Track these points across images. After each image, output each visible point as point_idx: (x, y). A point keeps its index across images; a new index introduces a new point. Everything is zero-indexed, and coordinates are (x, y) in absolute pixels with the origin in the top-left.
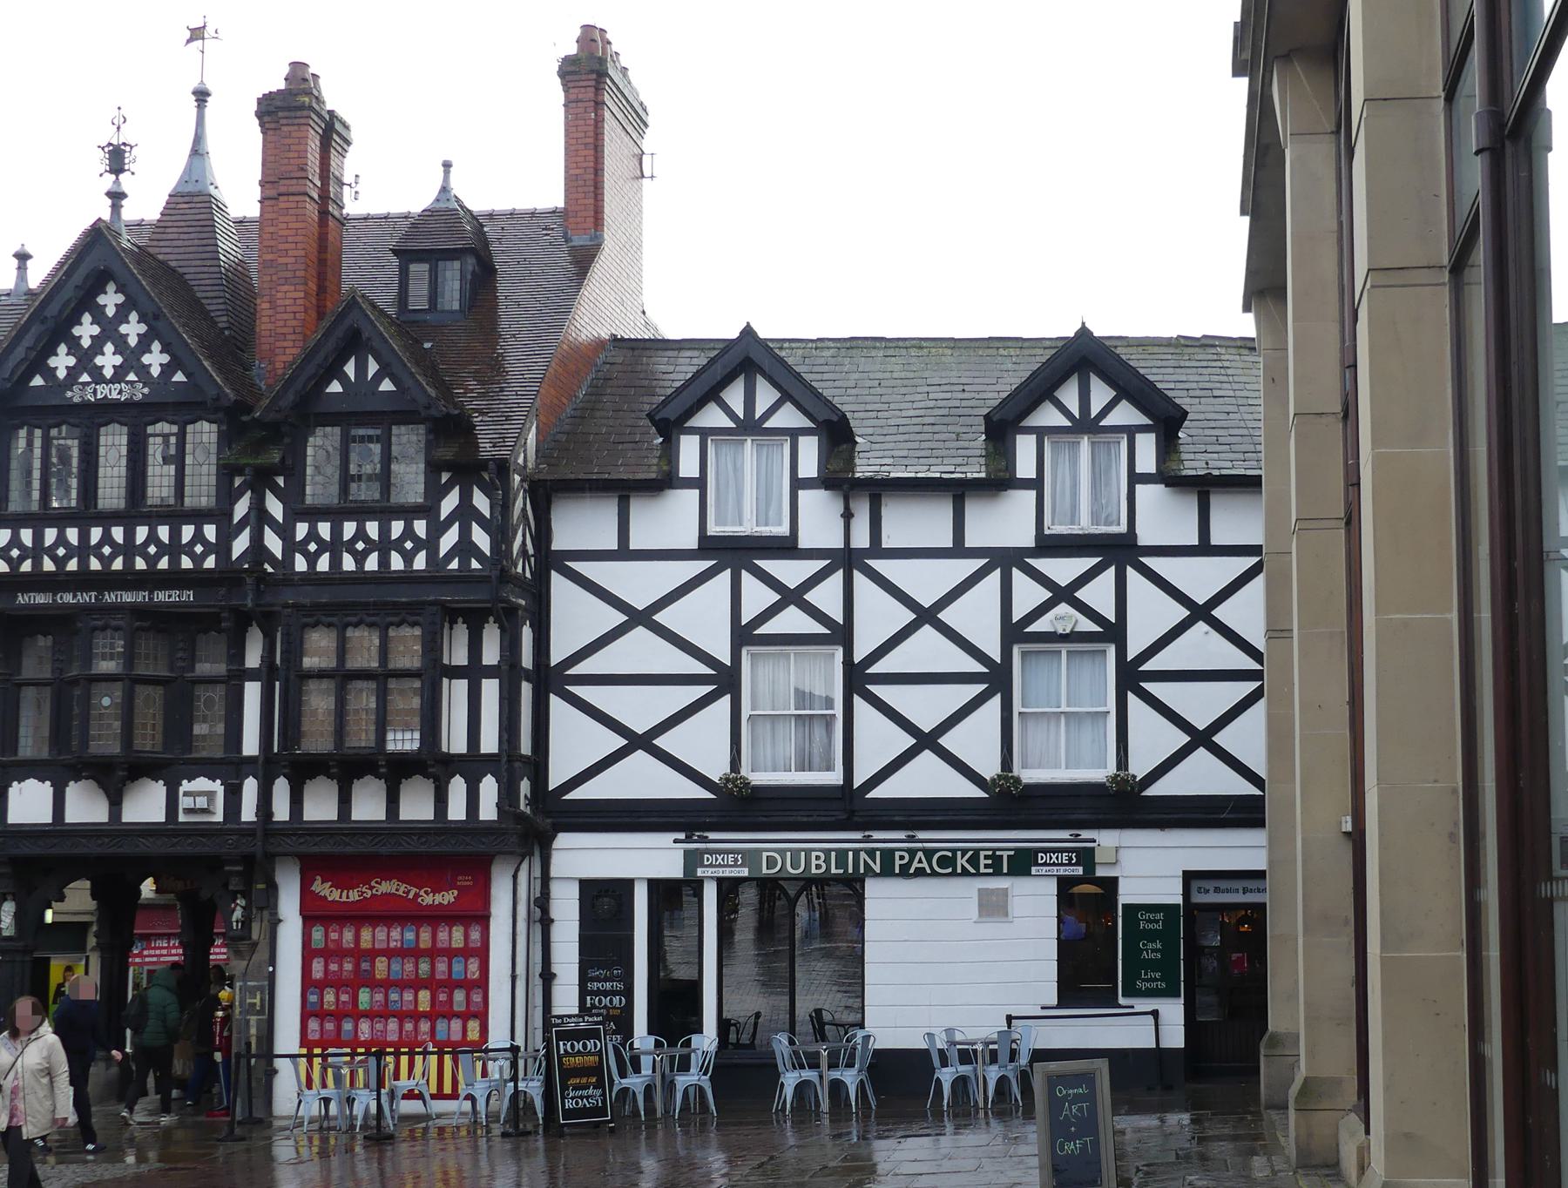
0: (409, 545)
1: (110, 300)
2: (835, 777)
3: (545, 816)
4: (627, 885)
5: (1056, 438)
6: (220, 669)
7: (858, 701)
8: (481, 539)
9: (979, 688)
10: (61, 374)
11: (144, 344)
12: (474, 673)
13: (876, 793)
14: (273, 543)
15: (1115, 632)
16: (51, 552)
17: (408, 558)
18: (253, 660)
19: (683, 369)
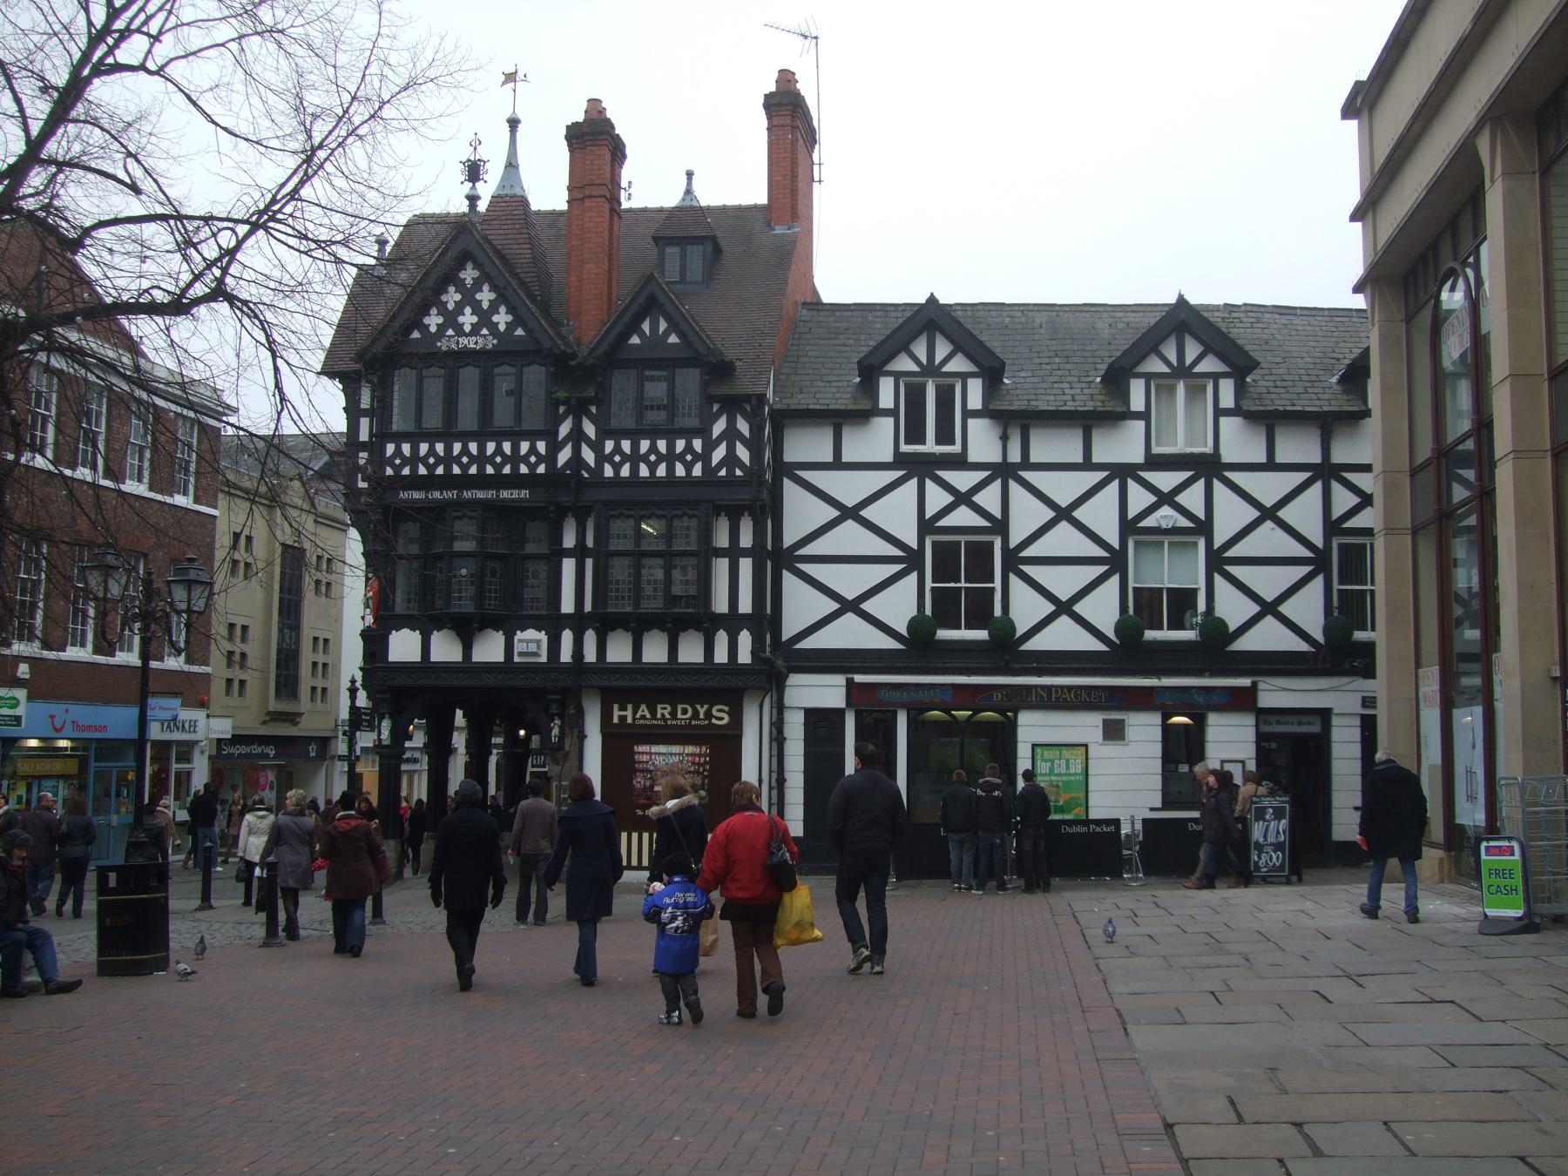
0: (498, 459)
1: (469, 275)
3: (782, 660)
5: (1161, 381)
6: (543, 549)
7: (1012, 577)
8: (743, 453)
9: (1307, 569)
10: (433, 329)
11: (494, 308)
12: (734, 553)
14: (588, 455)
15: (1204, 527)
16: (424, 461)
17: (689, 467)
18: (569, 541)
19: (881, 329)
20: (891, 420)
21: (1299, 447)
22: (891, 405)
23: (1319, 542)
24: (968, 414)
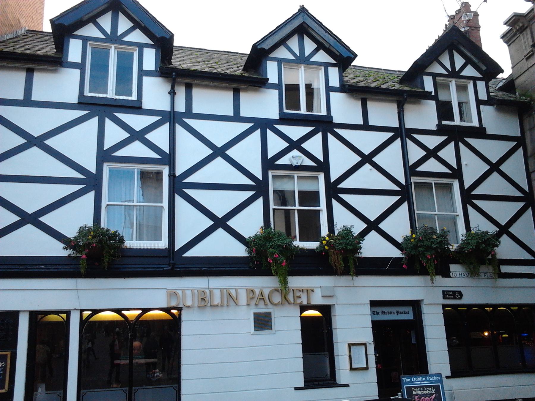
2: (163, 244)
4: (14, 315)
13: (190, 253)
20: (78, 72)
21: (383, 114)
22: (78, 60)
23: (402, 180)
24: (142, 73)
